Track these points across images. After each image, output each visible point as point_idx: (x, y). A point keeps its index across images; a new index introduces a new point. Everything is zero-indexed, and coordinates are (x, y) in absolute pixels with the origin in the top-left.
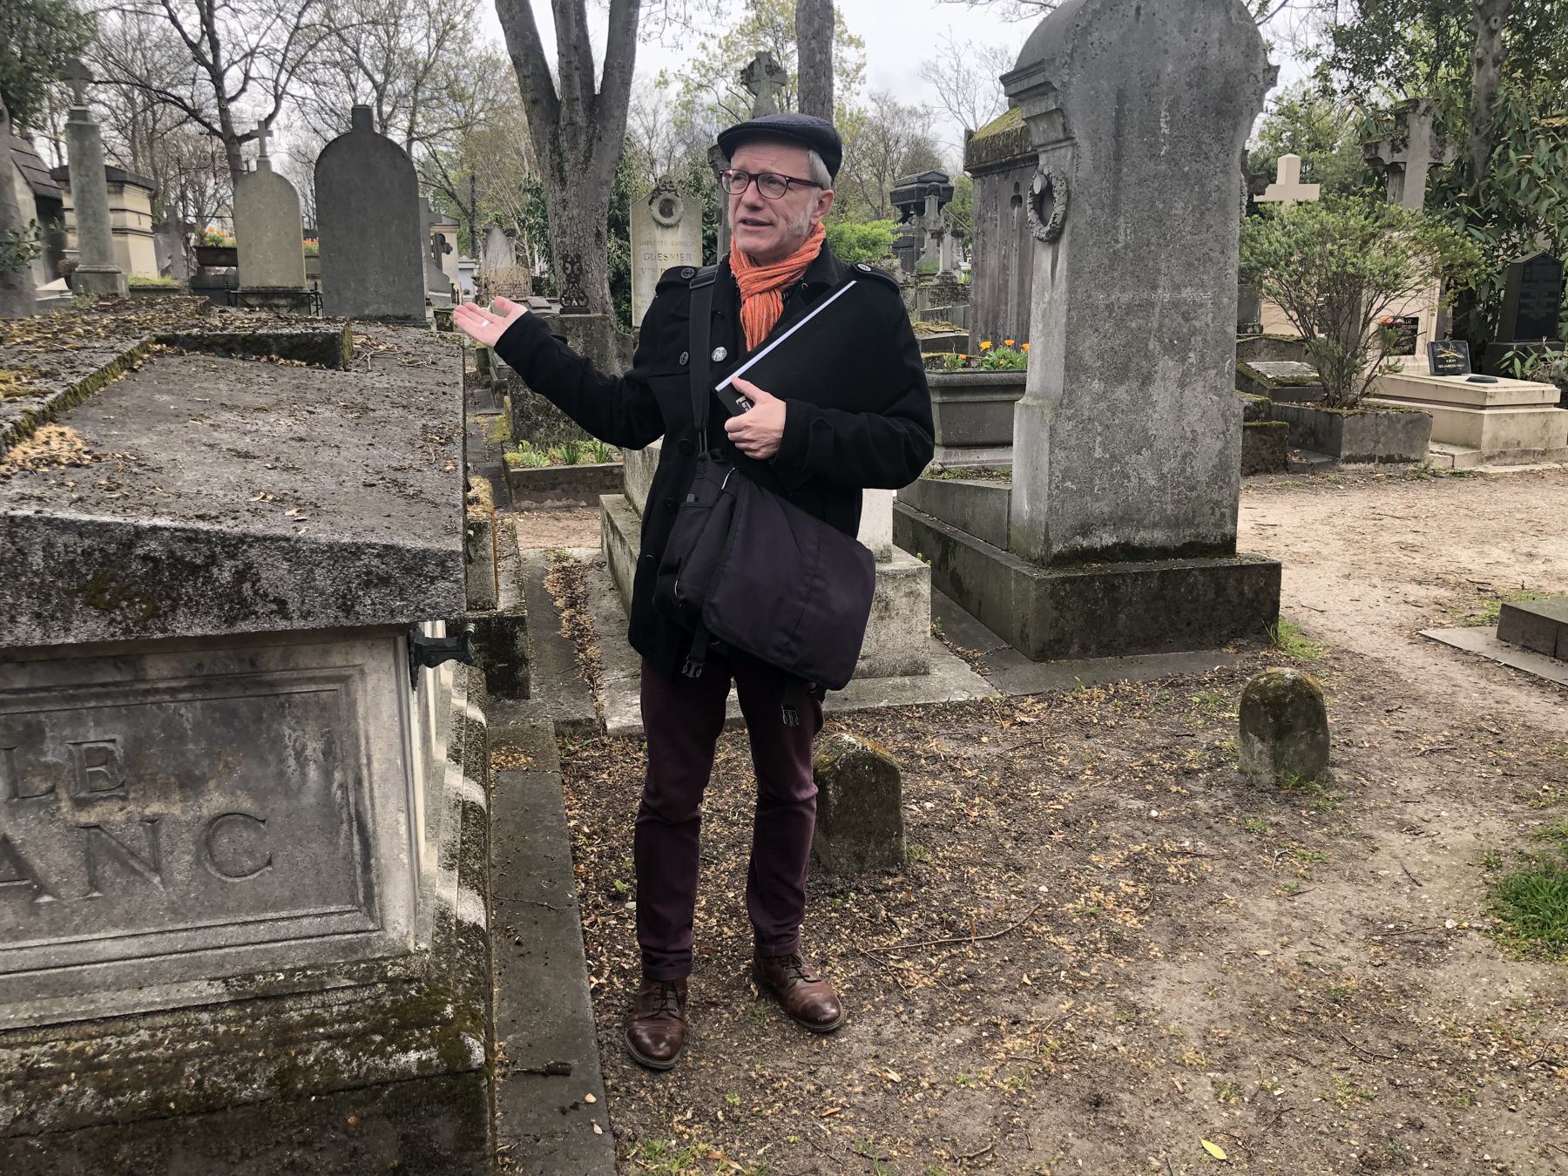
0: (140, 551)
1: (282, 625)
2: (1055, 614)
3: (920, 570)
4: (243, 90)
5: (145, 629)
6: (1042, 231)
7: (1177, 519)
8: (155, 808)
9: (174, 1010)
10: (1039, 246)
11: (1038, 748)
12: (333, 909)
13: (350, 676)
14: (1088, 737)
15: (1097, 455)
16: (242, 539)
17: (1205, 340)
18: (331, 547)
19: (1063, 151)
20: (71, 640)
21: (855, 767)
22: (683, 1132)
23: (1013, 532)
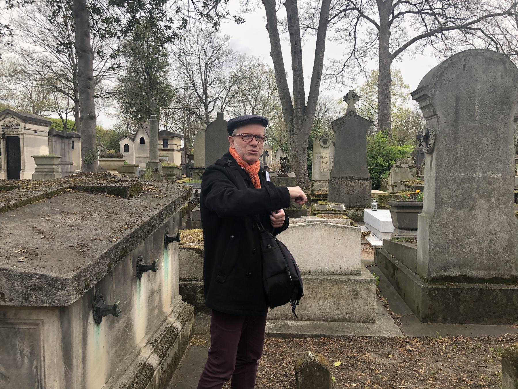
2: (431, 303)
3: (371, 280)
4: (213, 109)
6: (426, 149)
7: (489, 267)
10: (426, 155)
11: (412, 364)
13: (39, 324)
14: (437, 361)
15: (450, 238)
17: (499, 193)
18: (21, 274)
19: (434, 119)
21: (310, 368)
23: (418, 266)
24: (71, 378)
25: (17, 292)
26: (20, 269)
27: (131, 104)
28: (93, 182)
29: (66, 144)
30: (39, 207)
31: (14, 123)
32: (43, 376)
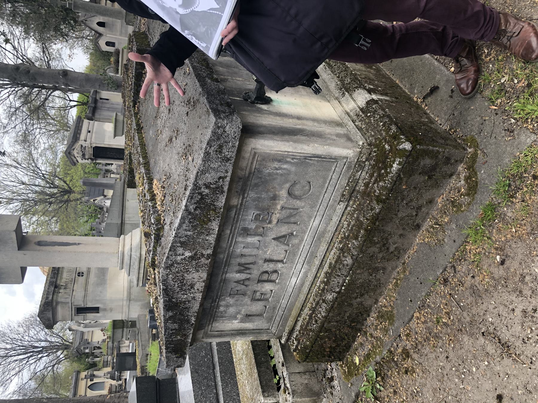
0: (193, 211)
1: (228, 179)
5: (219, 213)
8: (279, 207)
9: (342, 216)
12: (333, 169)
16: (195, 185)
18: (203, 161)
20: (217, 229)
22: (490, 59)
24: (312, 132)
25: (220, 166)
26: (199, 161)
27: (57, 29)
28: (130, 83)
29: (103, 106)
30: (149, 138)
31: (79, 149)
32: (301, 155)
